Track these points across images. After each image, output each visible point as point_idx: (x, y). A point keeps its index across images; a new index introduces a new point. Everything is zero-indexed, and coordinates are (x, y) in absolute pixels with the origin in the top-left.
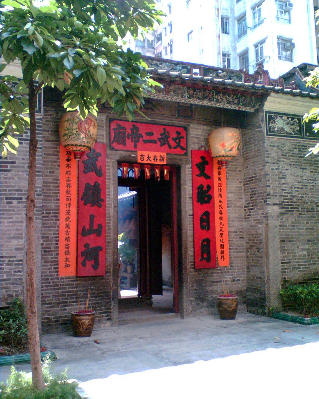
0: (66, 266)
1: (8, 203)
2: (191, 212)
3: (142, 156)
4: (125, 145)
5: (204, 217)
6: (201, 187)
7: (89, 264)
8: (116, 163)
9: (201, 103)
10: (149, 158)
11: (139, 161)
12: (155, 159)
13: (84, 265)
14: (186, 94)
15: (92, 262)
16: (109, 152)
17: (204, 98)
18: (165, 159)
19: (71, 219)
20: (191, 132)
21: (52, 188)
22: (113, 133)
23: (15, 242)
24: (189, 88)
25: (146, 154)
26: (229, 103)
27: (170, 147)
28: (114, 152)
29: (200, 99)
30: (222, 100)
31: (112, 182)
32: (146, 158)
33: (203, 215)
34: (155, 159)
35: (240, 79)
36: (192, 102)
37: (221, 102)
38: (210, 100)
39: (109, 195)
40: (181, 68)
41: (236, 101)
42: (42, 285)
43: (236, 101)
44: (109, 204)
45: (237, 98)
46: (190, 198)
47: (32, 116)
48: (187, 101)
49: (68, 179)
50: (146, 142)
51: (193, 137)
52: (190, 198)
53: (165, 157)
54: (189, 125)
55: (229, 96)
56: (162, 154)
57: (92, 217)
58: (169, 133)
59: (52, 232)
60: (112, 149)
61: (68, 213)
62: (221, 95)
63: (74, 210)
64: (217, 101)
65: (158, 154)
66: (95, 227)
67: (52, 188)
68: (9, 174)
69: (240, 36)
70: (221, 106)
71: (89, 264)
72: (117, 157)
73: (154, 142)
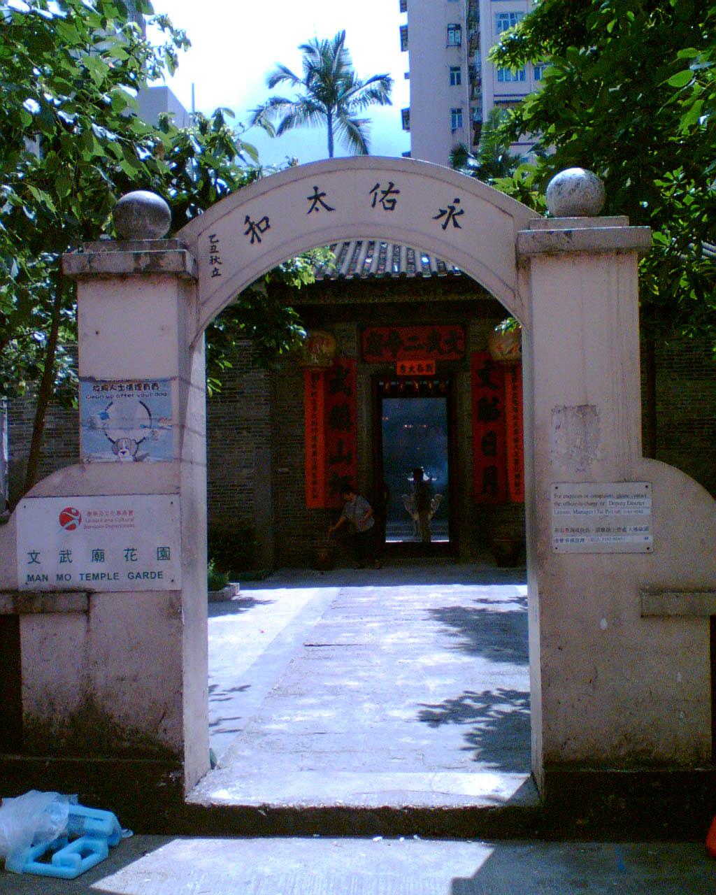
0: (314, 497)
1: (238, 433)
2: (470, 434)
3: (402, 367)
10: (411, 368)
12: (420, 367)
19: (318, 445)
23: (245, 472)
25: (408, 364)
29: (460, 293)
32: (408, 370)
34: (420, 367)
36: (449, 298)
39: (361, 417)
42: (131, 517)
44: (363, 427)
47: (659, 126)
48: (443, 299)
49: (314, 403)
53: (434, 365)
56: (429, 362)
59: (298, 461)
61: (314, 438)
63: (320, 437)
65: (424, 363)
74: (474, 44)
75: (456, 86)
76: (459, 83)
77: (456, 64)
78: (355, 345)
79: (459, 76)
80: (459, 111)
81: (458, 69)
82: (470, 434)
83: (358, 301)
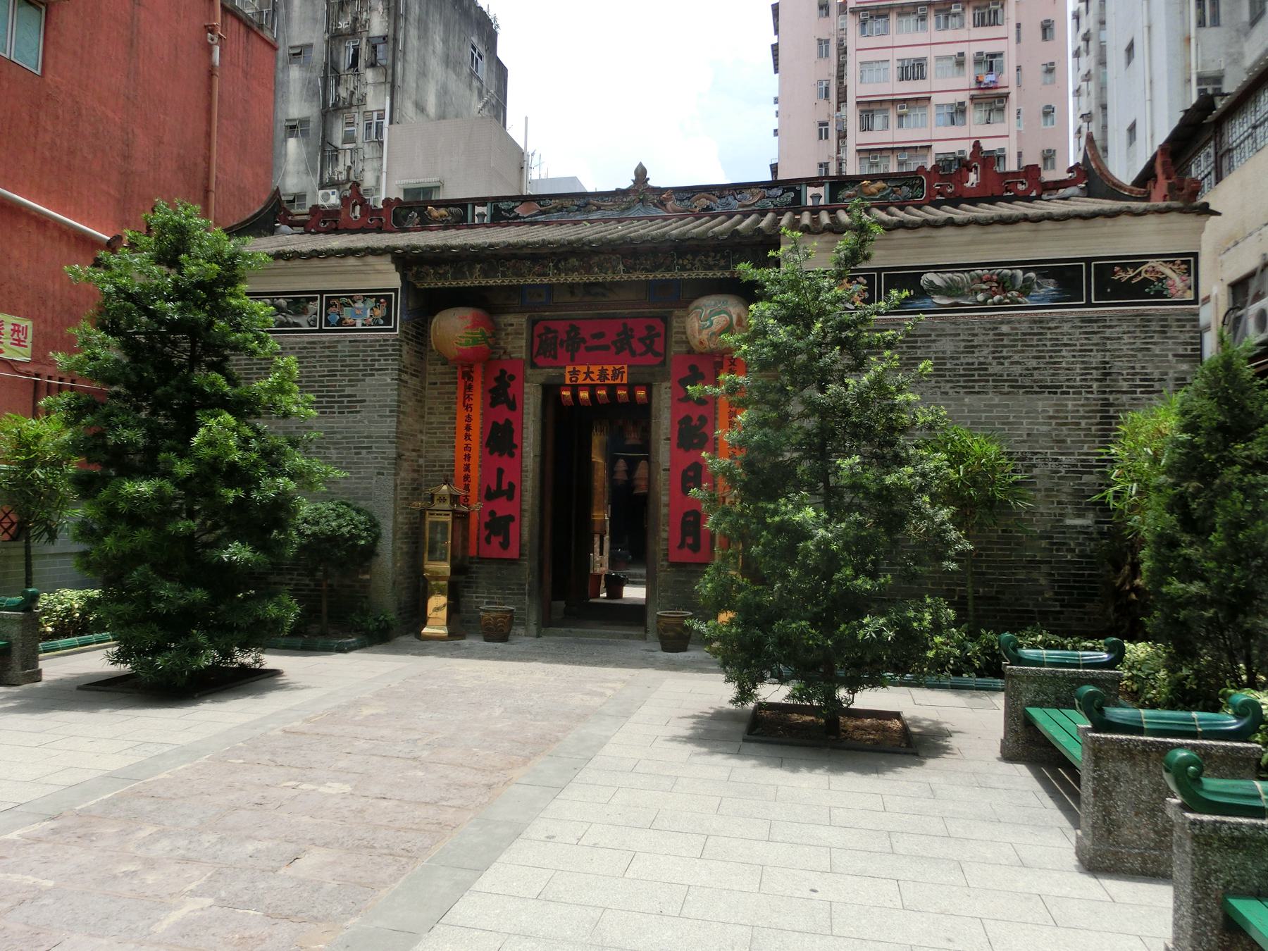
4: (555, 358)
5: (691, 474)
6: (687, 419)
7: (496, 540)
8: (540, 388)
9: (651, 277)
11: (568, 382)
13: (488, 540)
14: (621, 267)
15: (500, 539)
16: (529, 371)
17: (655, 268)
18: (625, 376)
20: (675, 324)
21: (1048, 343)
22: (537, 340)
24: (624, 257)
26: (710, 268)
27: (633, 353)
28: (539, 371)
29: (648, 271)
30: (693, 265)
31: (531, 417)
33: (689, 469)
35: (446, 279)
37: (691, 270)
38: (669, 269)
40: (780, 192)
41: (722, 263)
43: (722, 263)
45: (723, 257)
46: (668, 439)
50: (589, 349)
51: (678, 333)
52: (668, 439)
54: (671, 312)
55: (707, 256)
57: (500, 472)
58: (632, 330)
60: (533, 365)
62: (689, 256)
64: (683, 268)
66: (505, 487)
67: (1048, 343)
68: (358, 415)
69: (1254, 22)
70: (694, 276)
71: (496, 540)
72: (542, 379)
73: (607, 348)
74: (842, 98)
75: (824, 142)
76: (827, 137)
77: (824, 119)
78: (523, 343)
79: (827, 130)
80: (827, 124)
81: (827, 124)
82: (667, 465)
83: (515, 282)
